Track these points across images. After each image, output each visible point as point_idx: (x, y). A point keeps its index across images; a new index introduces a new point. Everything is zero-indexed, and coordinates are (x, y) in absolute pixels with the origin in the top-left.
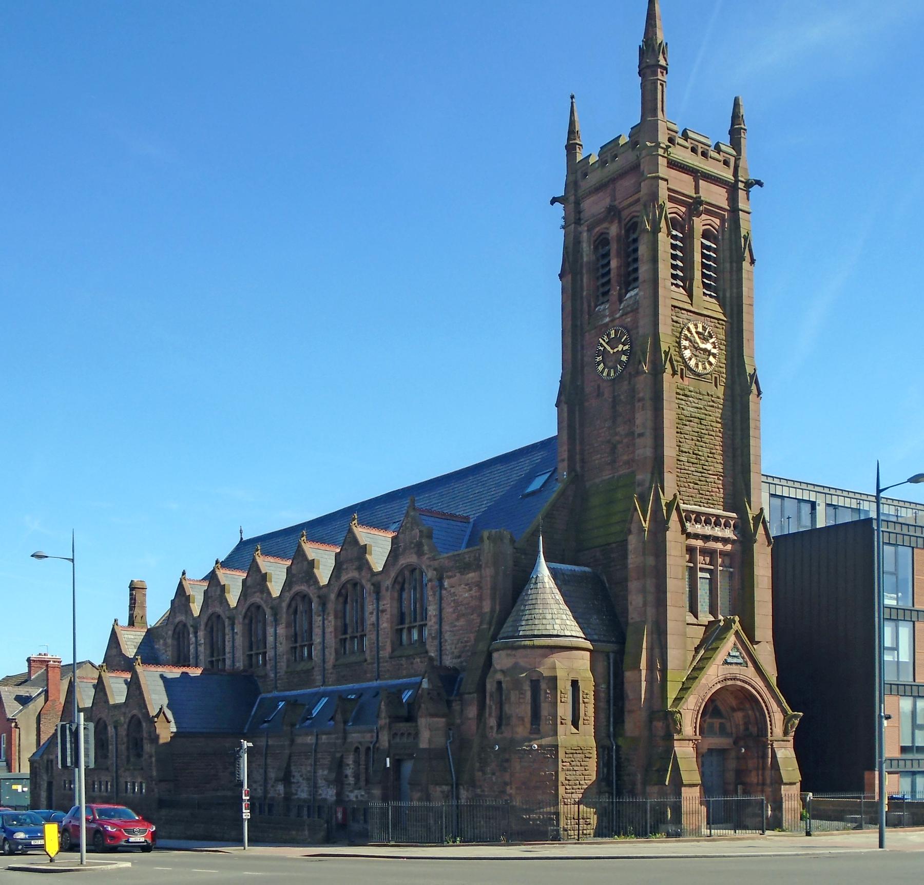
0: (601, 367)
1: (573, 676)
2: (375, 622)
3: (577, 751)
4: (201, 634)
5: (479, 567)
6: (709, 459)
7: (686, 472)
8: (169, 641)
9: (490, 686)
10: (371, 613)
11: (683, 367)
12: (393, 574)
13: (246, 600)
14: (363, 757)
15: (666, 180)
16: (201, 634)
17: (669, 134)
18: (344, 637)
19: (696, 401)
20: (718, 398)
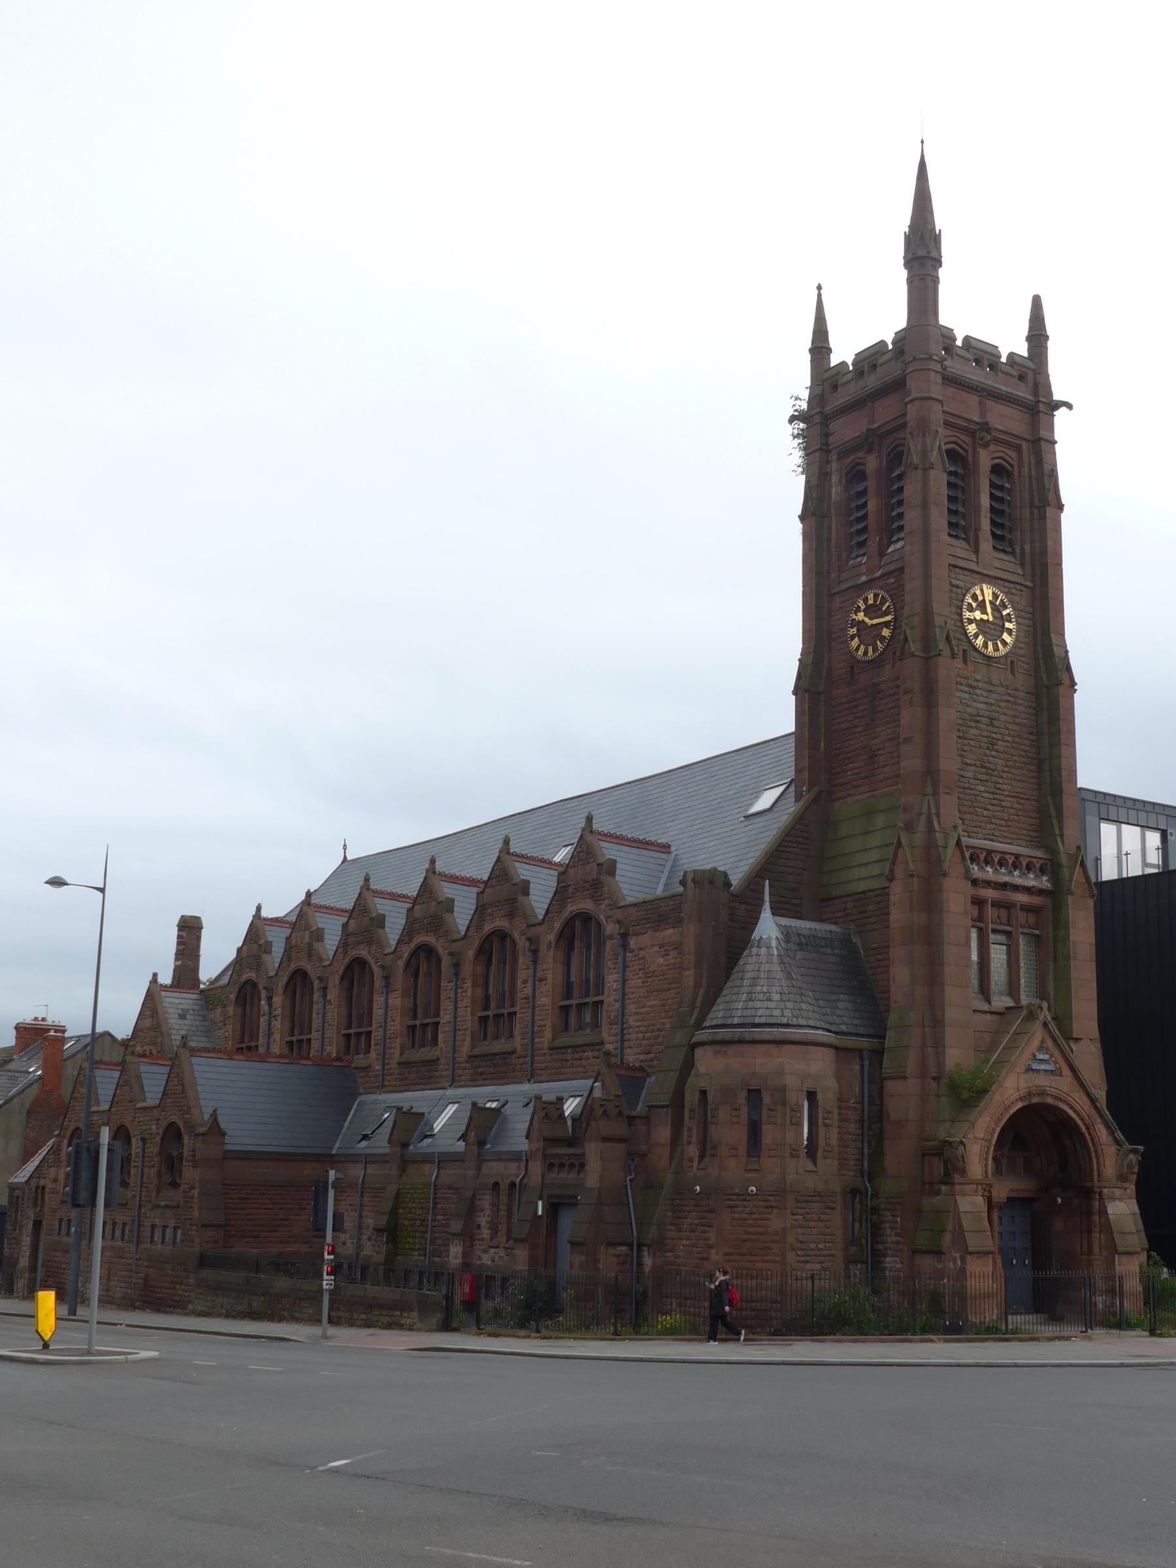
0: (855, 643)
1: (809, 1084)
2: (531, 996)
3: (815, 1199)
4: (277, 1000)
5: (679, 922)
6: (1004, 775)
7: (972, 792)
8: (231, 1010)
9: (691, 1099)
10: (525, 982)
11: (966, 648)
12: (557, 925)
13: (345, 952)
14: (504, 1199)
15: (941, 402)
16: (277, 1000)
17: (943, 342)
18: (485, 1014)
19: (985, 694)
20: (1016, 690)
